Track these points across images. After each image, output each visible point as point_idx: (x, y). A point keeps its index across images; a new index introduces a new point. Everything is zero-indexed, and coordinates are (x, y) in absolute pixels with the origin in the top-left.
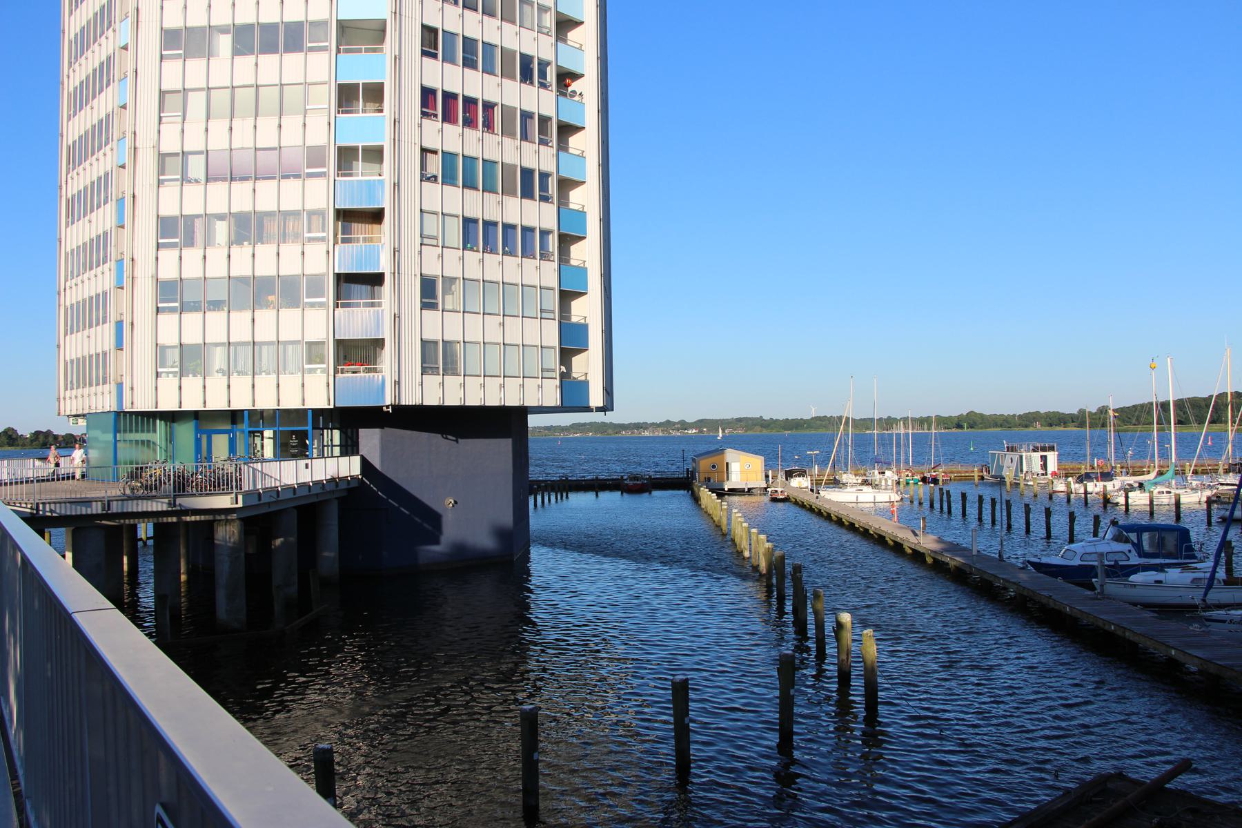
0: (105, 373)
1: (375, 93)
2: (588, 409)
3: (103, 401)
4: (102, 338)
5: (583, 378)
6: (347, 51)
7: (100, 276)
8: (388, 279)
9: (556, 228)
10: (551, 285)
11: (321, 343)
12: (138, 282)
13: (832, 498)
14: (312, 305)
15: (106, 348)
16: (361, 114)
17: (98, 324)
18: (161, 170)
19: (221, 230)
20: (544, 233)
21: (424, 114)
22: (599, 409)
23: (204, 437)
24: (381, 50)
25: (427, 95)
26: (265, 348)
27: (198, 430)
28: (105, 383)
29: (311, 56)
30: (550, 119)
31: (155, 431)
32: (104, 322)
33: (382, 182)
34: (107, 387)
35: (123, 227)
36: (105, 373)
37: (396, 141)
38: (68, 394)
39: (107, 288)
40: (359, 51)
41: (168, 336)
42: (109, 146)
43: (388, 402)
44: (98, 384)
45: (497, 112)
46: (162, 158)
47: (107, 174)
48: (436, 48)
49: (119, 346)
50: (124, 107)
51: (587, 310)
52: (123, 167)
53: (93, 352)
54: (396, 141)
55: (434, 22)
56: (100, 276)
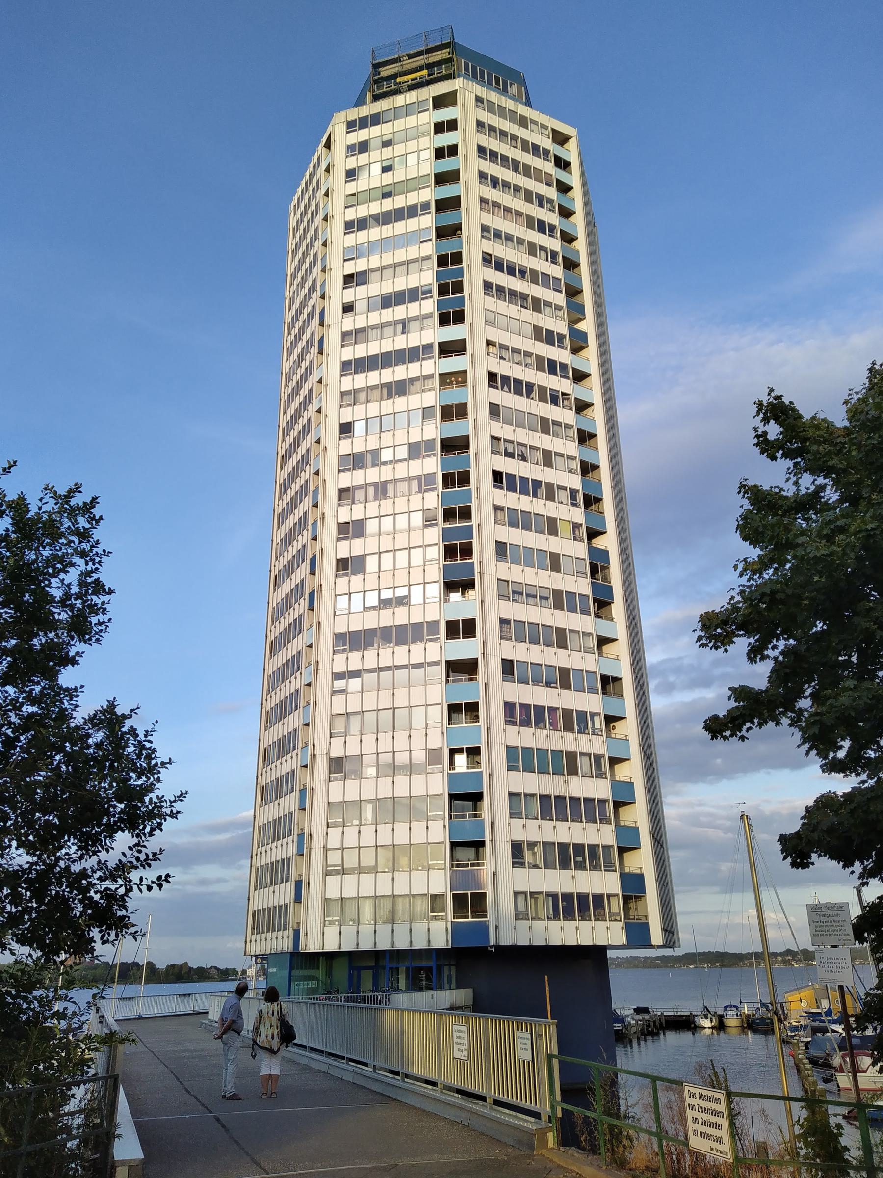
0: (285, 921)
1: (472, 709)
2: (652, 947)
3: (282, 942)
4: (284, 893)
5: (638, 871)
6: (454, 681)
7: (285, 846)
8: (488, 844)
9: (584, 523)
10: (583, 557)
11: (443, 896)
12: (314, 851)
13: (875, 1104)
14: (430, 640)
15: (287, 901)
16: (464, 725)
17: (282, 882)
18: (326, 912)
19: (368, 812)
20: (602, 802)
21: (507, 722)
22: (659, 947)
23: (356, 973)
24: (483, 865)
25: (509, 707)
26: (400, 900)
27: (351, 967)
28: (285, 929)
29: (423, 302)
30: (578, 491)
31: (318, 968)
32: (287, 881)
33: (481, 772)
34: (291, 838)
35: (304, 809)
36: (285, 921)
37: (465, 140)
38: (259, 850)
39: (290, 854)
40: (461, 680)
41: (333, 893)
42: (295, 752)
43: (492, 944)
44: (279, 930)
45: (536, 389)
46: (326, 901)
47: (297, 691)
48: (502, 483)
49: (298, 899)
50: (307, 725)
51: (609, 542)
52: (306, 766)
53: (276, 904)
54: (465, 140)
55: (494, 370)
56: (285, 846)
